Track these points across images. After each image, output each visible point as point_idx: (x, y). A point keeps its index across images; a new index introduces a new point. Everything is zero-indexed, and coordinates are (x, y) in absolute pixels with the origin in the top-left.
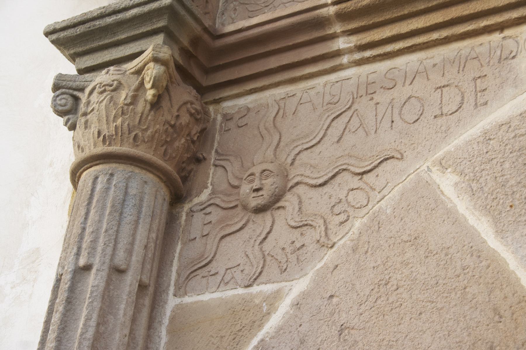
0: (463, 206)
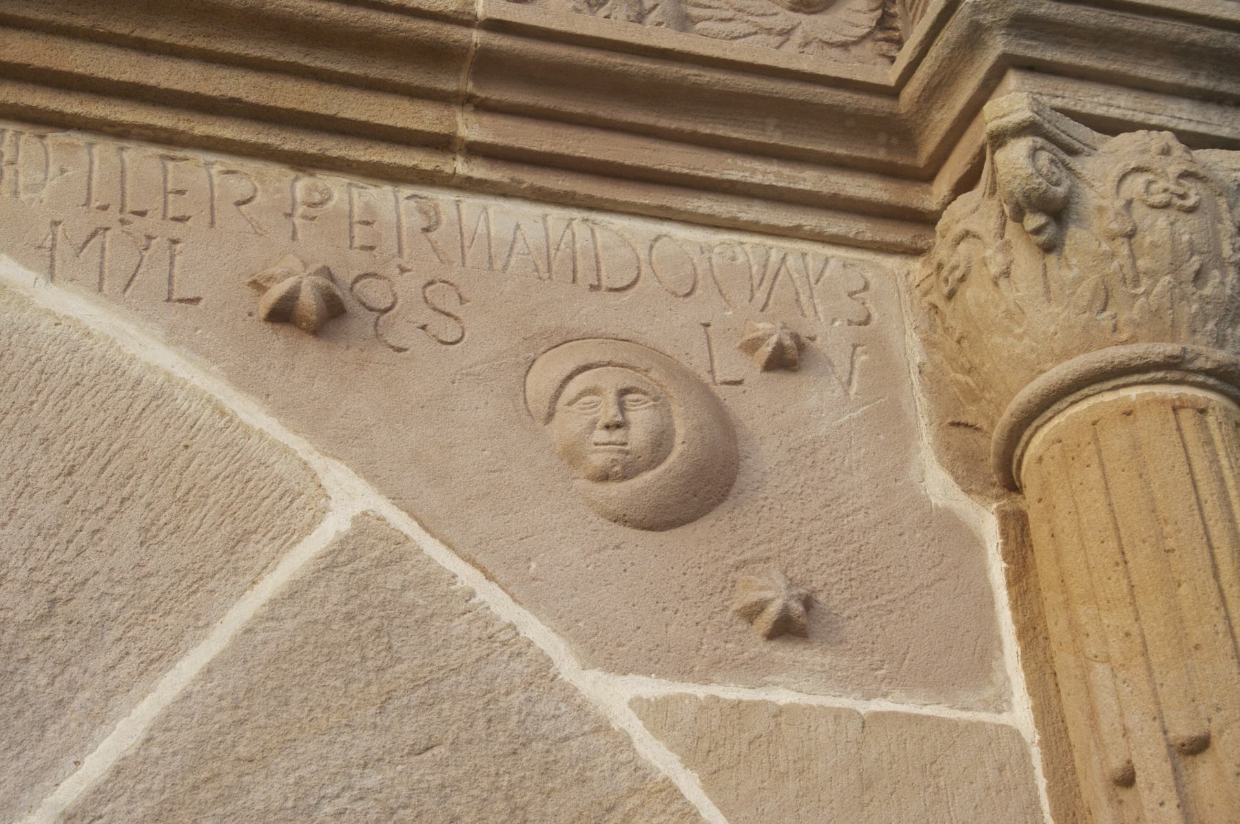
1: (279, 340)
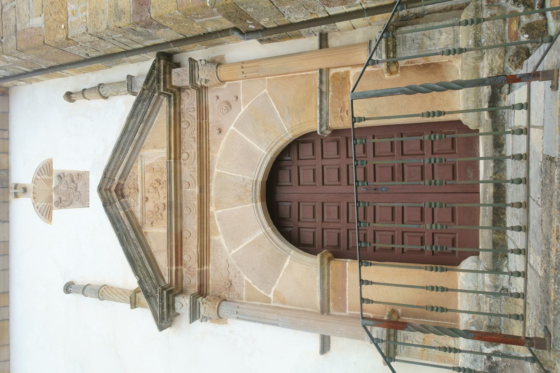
0: (237, 249)
1: (222, 132)
